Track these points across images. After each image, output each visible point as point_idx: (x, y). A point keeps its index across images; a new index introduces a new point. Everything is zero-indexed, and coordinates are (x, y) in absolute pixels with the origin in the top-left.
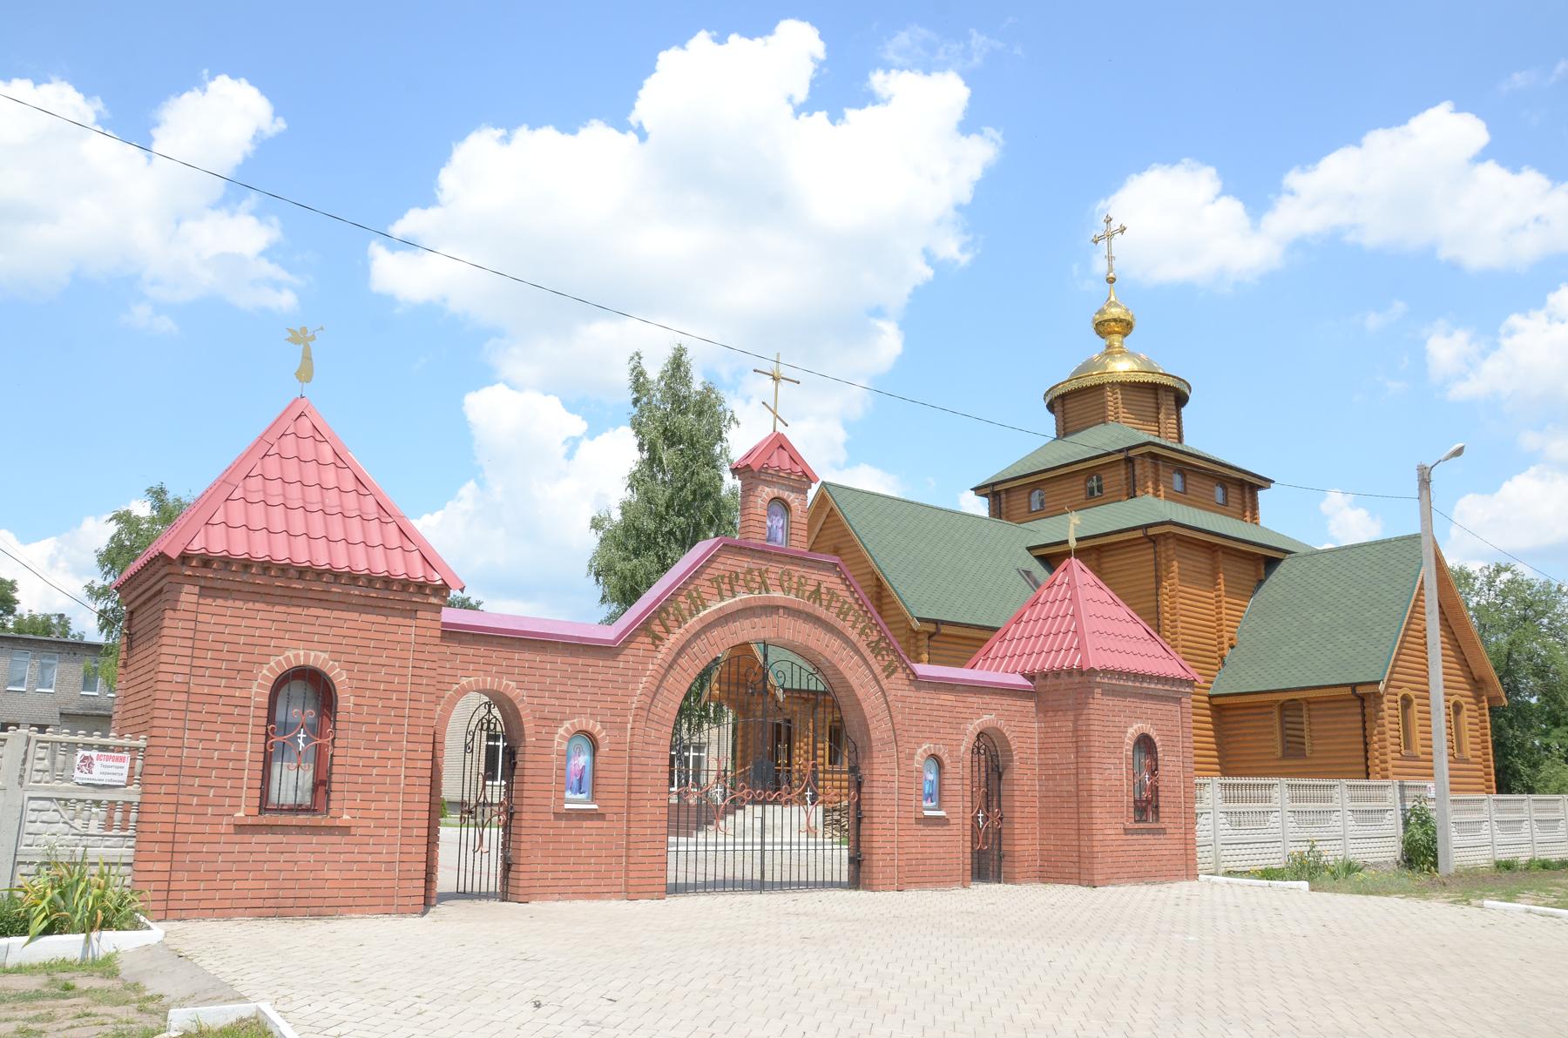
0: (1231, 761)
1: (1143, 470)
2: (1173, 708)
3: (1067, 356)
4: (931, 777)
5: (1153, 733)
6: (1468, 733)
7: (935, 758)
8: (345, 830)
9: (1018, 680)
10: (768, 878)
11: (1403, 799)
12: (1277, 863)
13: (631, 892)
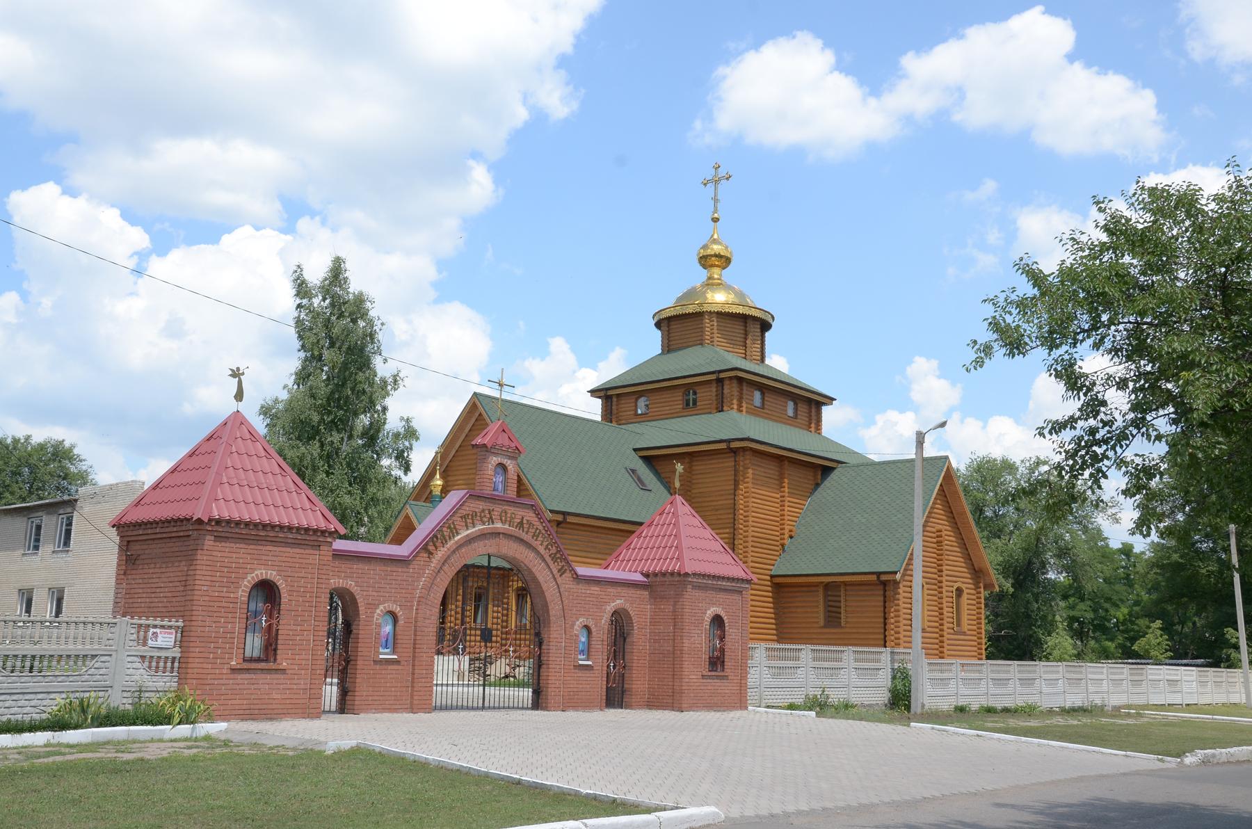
0: (786, 630)
1: (730, 390)
2: (736, 597)
3: (673, 284)
4: (583, 639)
5: (723, 614)
6: (966, 607)
7: (587, 628)
8: (283, 671)
9: (638, 577)
10: (487, 704)
11: (893, 661)
12: (799, 701)
13: (412, 709)
